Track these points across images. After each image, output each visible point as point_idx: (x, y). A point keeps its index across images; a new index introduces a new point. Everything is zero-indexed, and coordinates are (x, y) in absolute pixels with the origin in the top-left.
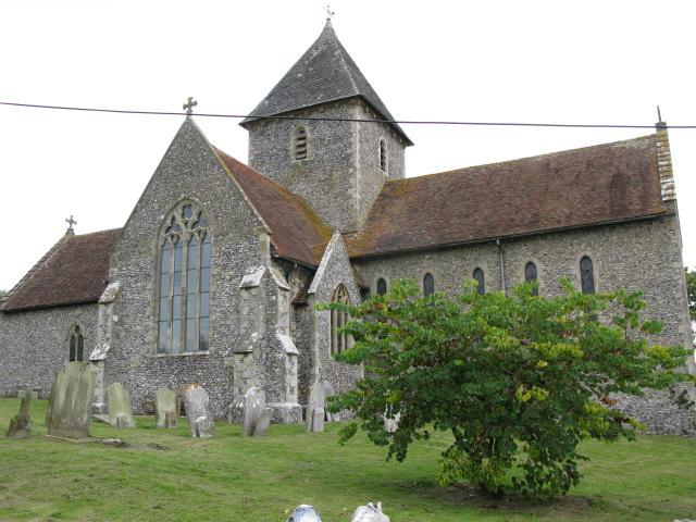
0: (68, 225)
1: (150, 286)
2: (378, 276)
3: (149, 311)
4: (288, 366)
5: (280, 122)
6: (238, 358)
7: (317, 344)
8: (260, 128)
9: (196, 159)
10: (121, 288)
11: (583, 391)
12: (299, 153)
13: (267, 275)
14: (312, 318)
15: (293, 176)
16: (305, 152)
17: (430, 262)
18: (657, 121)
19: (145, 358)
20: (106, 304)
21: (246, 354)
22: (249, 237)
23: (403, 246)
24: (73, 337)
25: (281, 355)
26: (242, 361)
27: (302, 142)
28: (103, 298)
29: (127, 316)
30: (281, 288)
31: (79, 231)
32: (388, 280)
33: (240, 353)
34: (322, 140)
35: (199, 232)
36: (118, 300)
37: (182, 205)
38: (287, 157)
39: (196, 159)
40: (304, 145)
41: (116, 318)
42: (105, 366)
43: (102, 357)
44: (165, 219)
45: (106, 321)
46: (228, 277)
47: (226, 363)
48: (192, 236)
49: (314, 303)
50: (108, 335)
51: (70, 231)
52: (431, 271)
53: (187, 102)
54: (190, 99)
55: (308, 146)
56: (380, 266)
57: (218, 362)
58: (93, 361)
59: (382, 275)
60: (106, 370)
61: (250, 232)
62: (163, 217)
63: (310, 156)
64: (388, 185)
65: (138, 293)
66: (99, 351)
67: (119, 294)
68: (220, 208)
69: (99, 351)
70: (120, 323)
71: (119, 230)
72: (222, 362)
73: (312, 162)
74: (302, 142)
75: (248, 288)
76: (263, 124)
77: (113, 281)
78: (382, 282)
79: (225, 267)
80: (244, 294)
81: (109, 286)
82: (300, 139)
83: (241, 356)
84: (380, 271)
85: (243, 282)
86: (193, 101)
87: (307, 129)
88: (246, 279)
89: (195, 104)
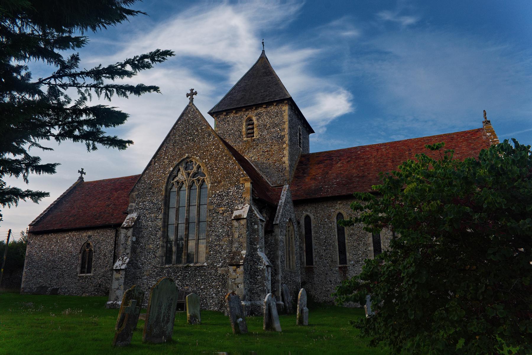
0: (80, 175)
1: (161, 216)
2: (305, 213)
3: (160, 233)
4: (266, 274)
5: (236, 113)
6: (231, 269)
7: (279, 259)
8: (222, 117)
9: (197, 131)
10: (139, 218)
11: (136, 263)
12: (249, 134)
13: (250, 210)
14: (276, 240)
15: (245, 148)
16: (253, 133)
17: (341, 206)
18: (484, 120)
19: (156, 268)
20: (127, 228)
21: (238, 266)
22: (237, 184)
23: (323, 194)
24: (85, 251)
25: (262, 267)
26: (235, 271)
27: (250, 127)
28: (125, 224)
29: (143, 237)
30: (261, 220)
31: (87, 179)
32: (312, 217)
33: (234, 265)
34: (265, 126)
35: (199, 180)
36: (137, 226)
37: (186, 161)
38: (240, 136)
39: (197, 131)
40: (253, 129)
41: (134, 239)
42: (126, 274)
43: (123, 267)
44: (173, 170)
45: (126, 240)
46: (221, 212)
47: (219, 272)
48: (193, 182)
49: (277, 231)
50: (128, 251)
51: (81, 178)
52: (342, 211)
53: (189, 92)
54: (192, 90)
55: (255, 129)
56: (306, 207)
57: (213, 271)
58: (116, 270)
59: (308, 214)
60: (126, 277)
61: (238, 181)
62: (171, 169)
63: (256, 135)
64: (303, 156)
65: (152, 221)
66: (120, 263)
67: (137, 221)
68: (216, 164)
69: (120, 263)
70: (137, 242)
71: (140, 175)
72: (216, 270)
73: (258, 139)
74: (250, 127)
75: (238, 219)
76: (224, 114)
77: (131, 212)
78: (307, 218)
79: (219, 205)
80: (235, 223)
81: (129, 217)
82: (249, 125)
83: (235, 267)
84: (307, 211)
85: (234, 215)
86: (194, 91)
87: (254, 119)
88: (236, 213)
89: (196, 93)
